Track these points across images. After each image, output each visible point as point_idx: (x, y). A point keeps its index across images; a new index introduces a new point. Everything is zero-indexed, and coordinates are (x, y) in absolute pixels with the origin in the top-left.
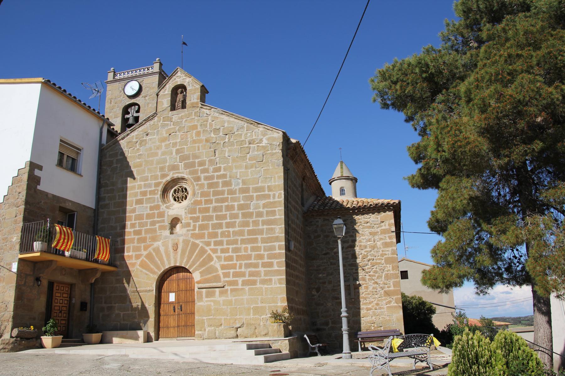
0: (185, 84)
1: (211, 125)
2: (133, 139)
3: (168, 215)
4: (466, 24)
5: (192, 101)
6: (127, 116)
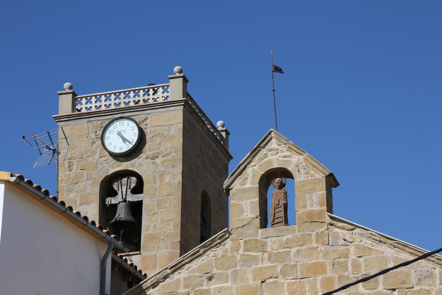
0: (290, 169)
1: (356, 266)
2: (178, 287)
5: (309, 208)
6: (113, 201)
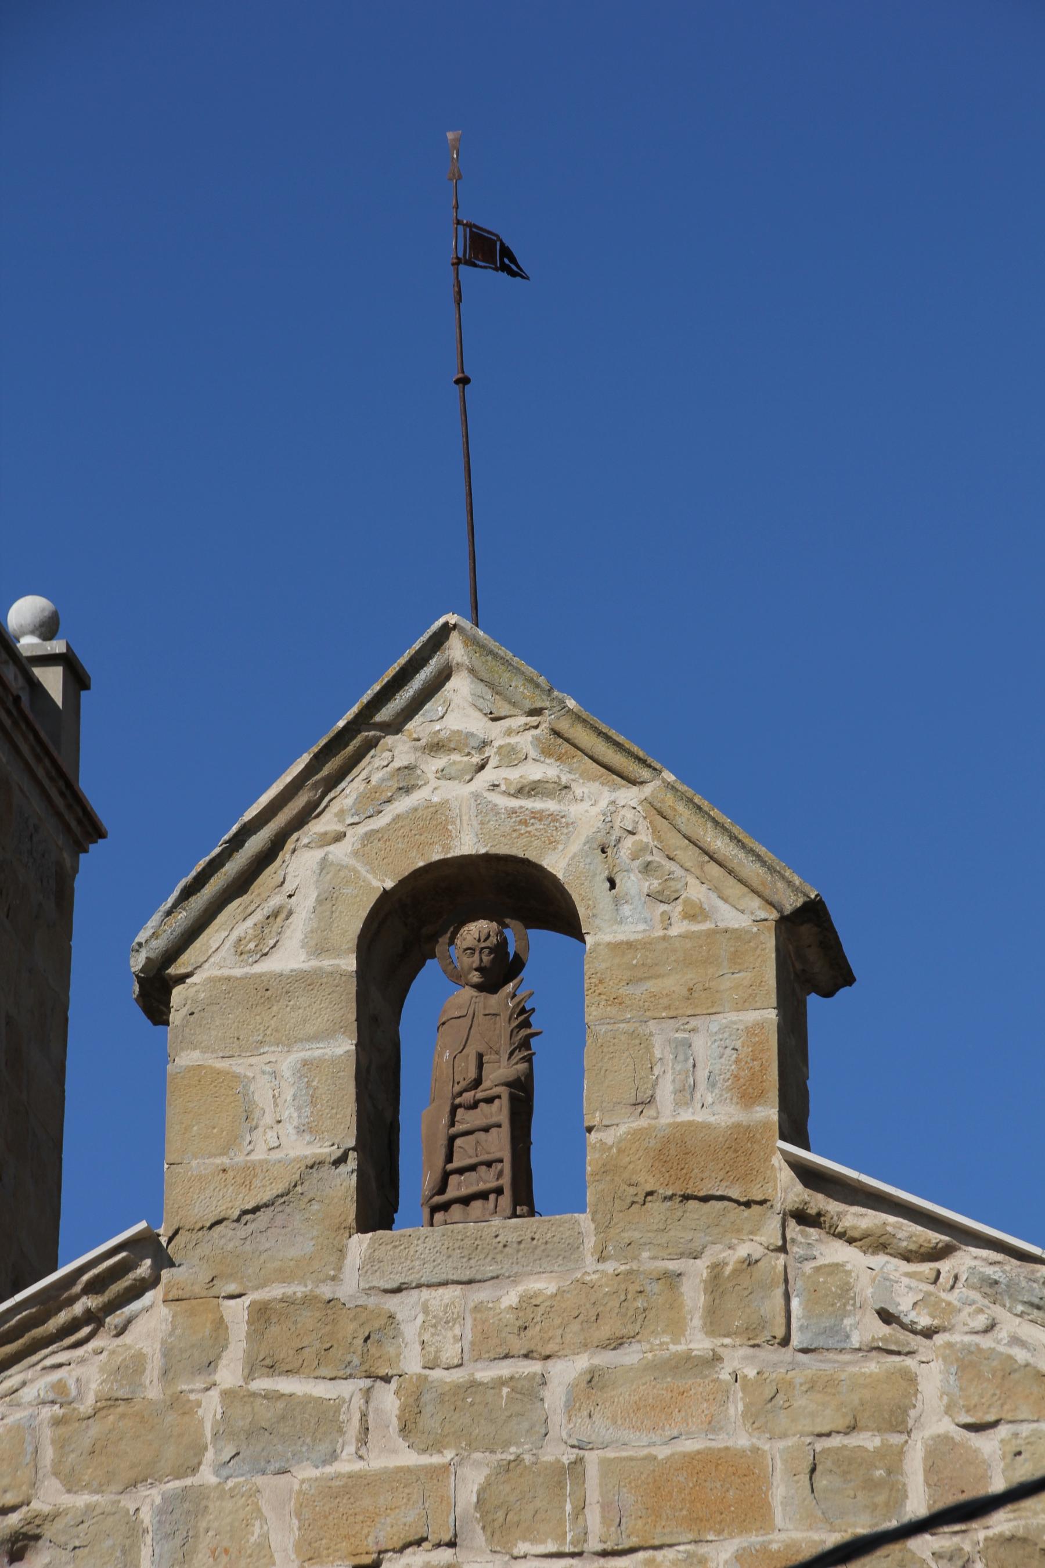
5: (668, 1113)
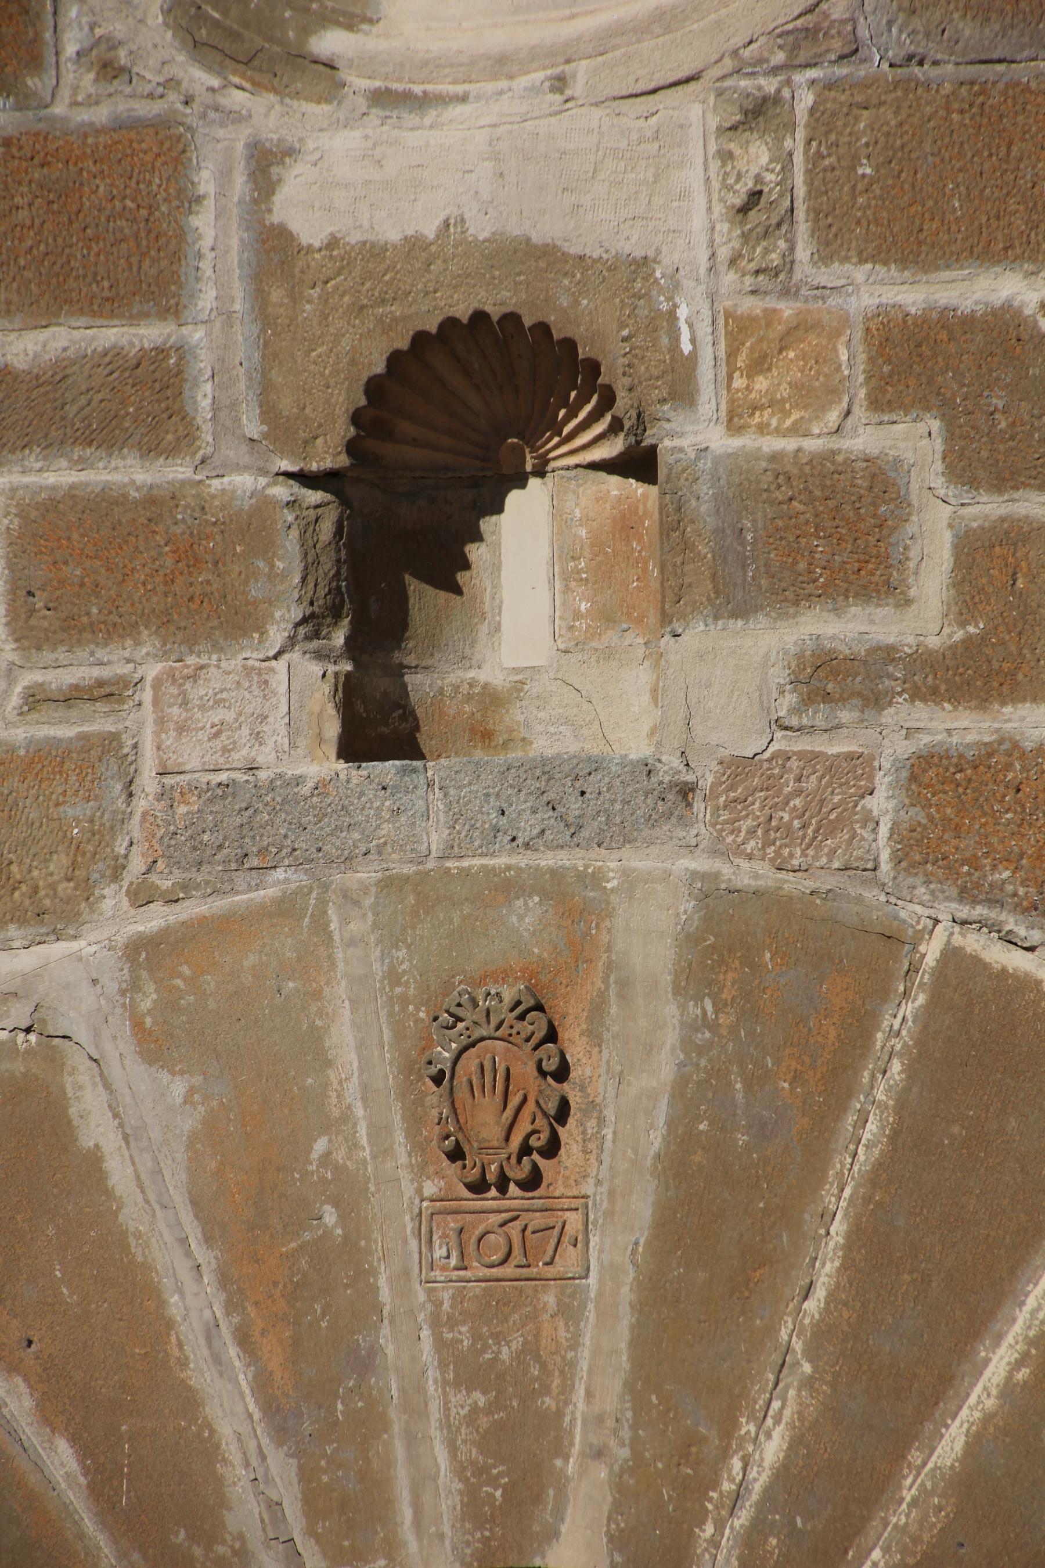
3: (274, 252)
4: (1027, 1336)
